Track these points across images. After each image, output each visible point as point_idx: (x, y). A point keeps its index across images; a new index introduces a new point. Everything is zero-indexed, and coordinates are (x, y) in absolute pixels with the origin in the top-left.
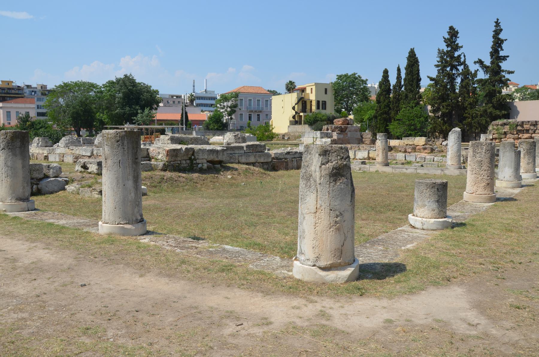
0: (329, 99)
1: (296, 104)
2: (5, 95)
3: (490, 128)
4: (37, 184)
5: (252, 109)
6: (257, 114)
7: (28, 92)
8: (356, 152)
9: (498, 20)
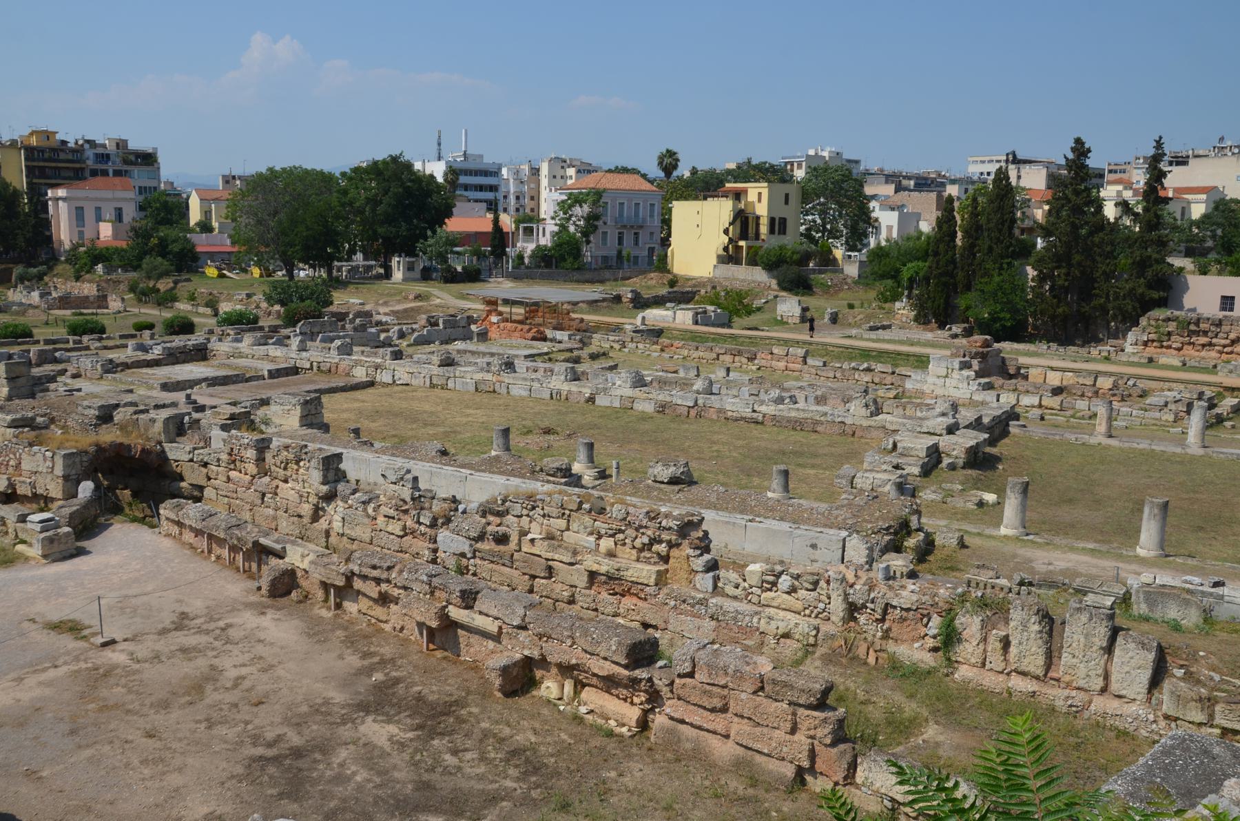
1: (730, 224)
2: (46, 164)
3: (1143, 321)
5: (625, 222)
6: (633, 231)
7: (92, 157)
8: (1021, 397)
9: (1161, 138)
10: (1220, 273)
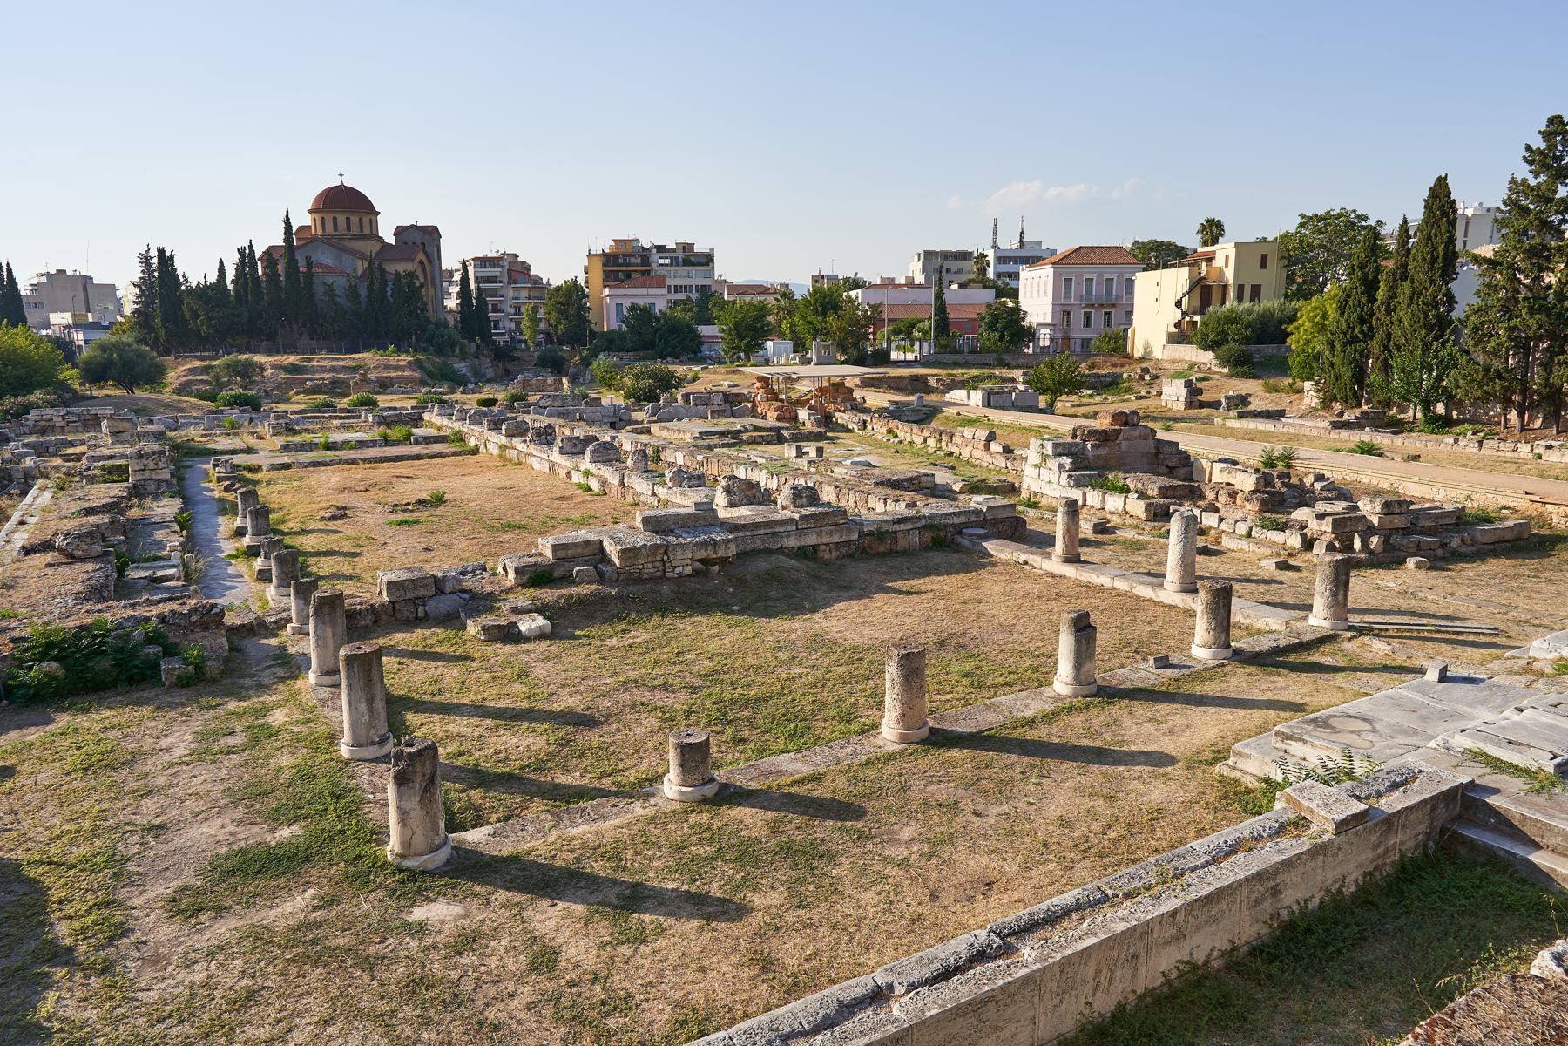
0: (1271, 278)
4: (424, 605)
10: (1516, 185)
